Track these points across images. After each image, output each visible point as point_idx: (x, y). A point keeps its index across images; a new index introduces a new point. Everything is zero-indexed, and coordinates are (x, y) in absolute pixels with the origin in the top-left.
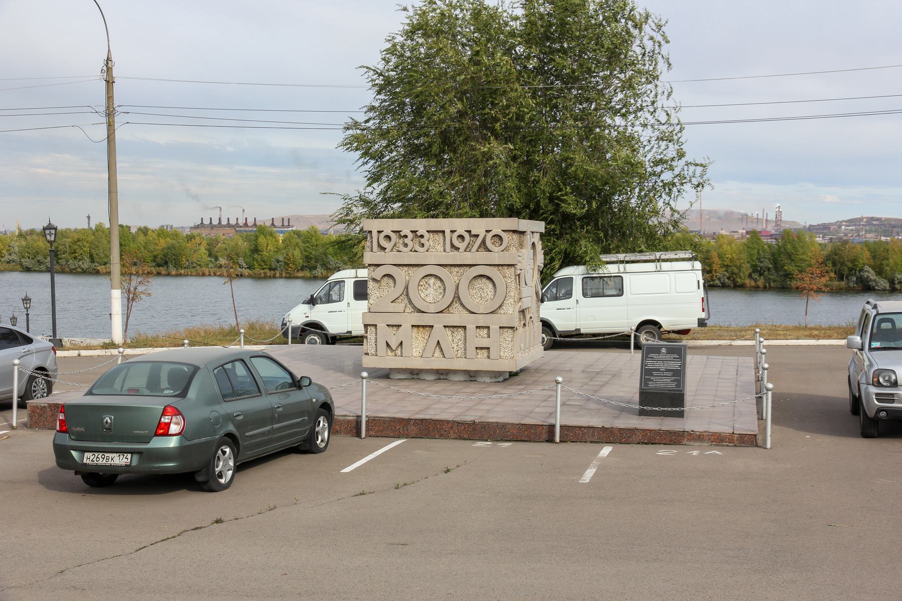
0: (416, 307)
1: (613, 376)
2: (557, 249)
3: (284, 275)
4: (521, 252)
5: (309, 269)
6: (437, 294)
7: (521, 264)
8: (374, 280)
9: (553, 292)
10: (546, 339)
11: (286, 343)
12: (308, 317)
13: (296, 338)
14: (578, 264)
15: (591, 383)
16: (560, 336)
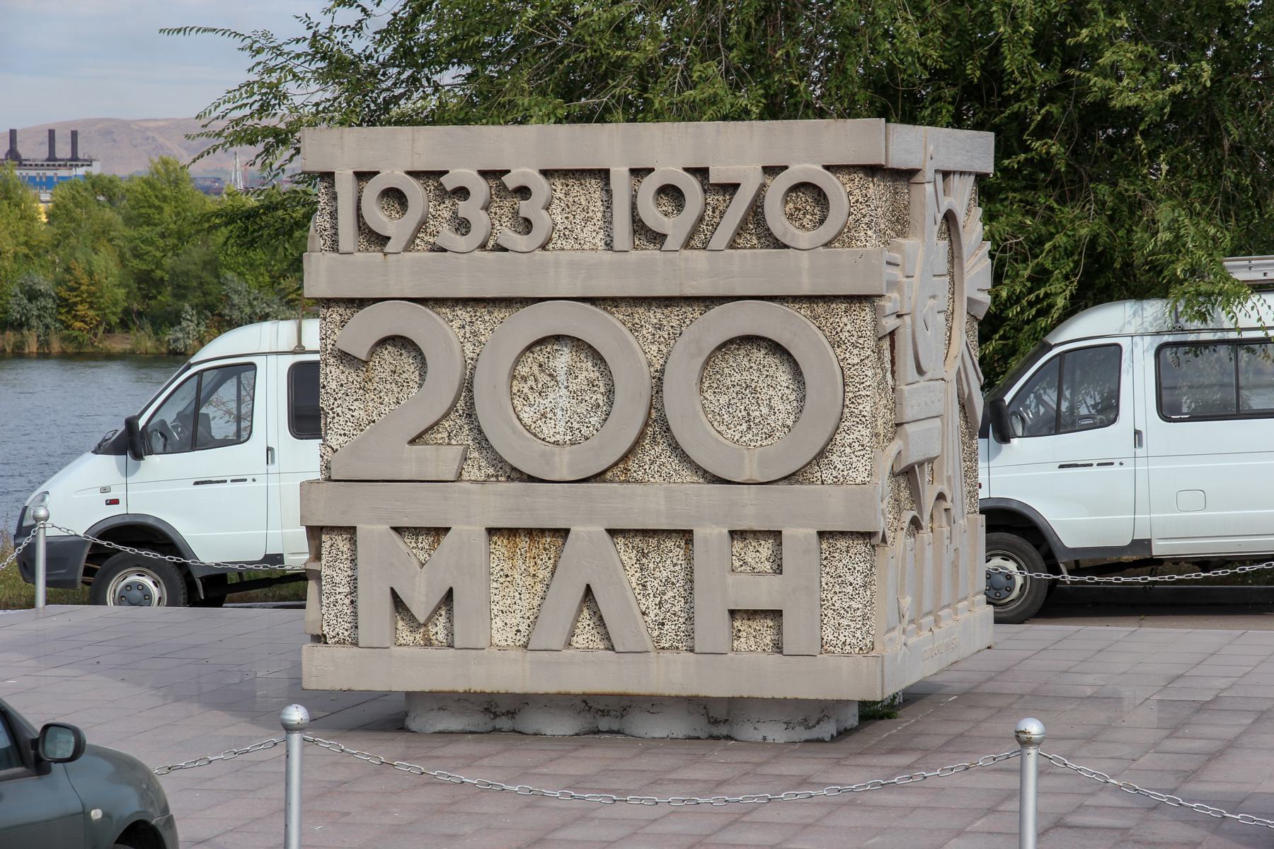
0: (502, 460)
1: (1256, 721)
2: (1060, 239)
3: (56, 346)
4: (899, 249)
5: (153, 324)
6: (582, 409)
7: (900, 291)
8: (344, 357)
9: (1045, 404)
10: (1019, 580)
11: (31, 604)
12: (115, 502)
13: (72, 584)
14: (1140, 293)
15: (1170, 745)
16: (1076, 569)
